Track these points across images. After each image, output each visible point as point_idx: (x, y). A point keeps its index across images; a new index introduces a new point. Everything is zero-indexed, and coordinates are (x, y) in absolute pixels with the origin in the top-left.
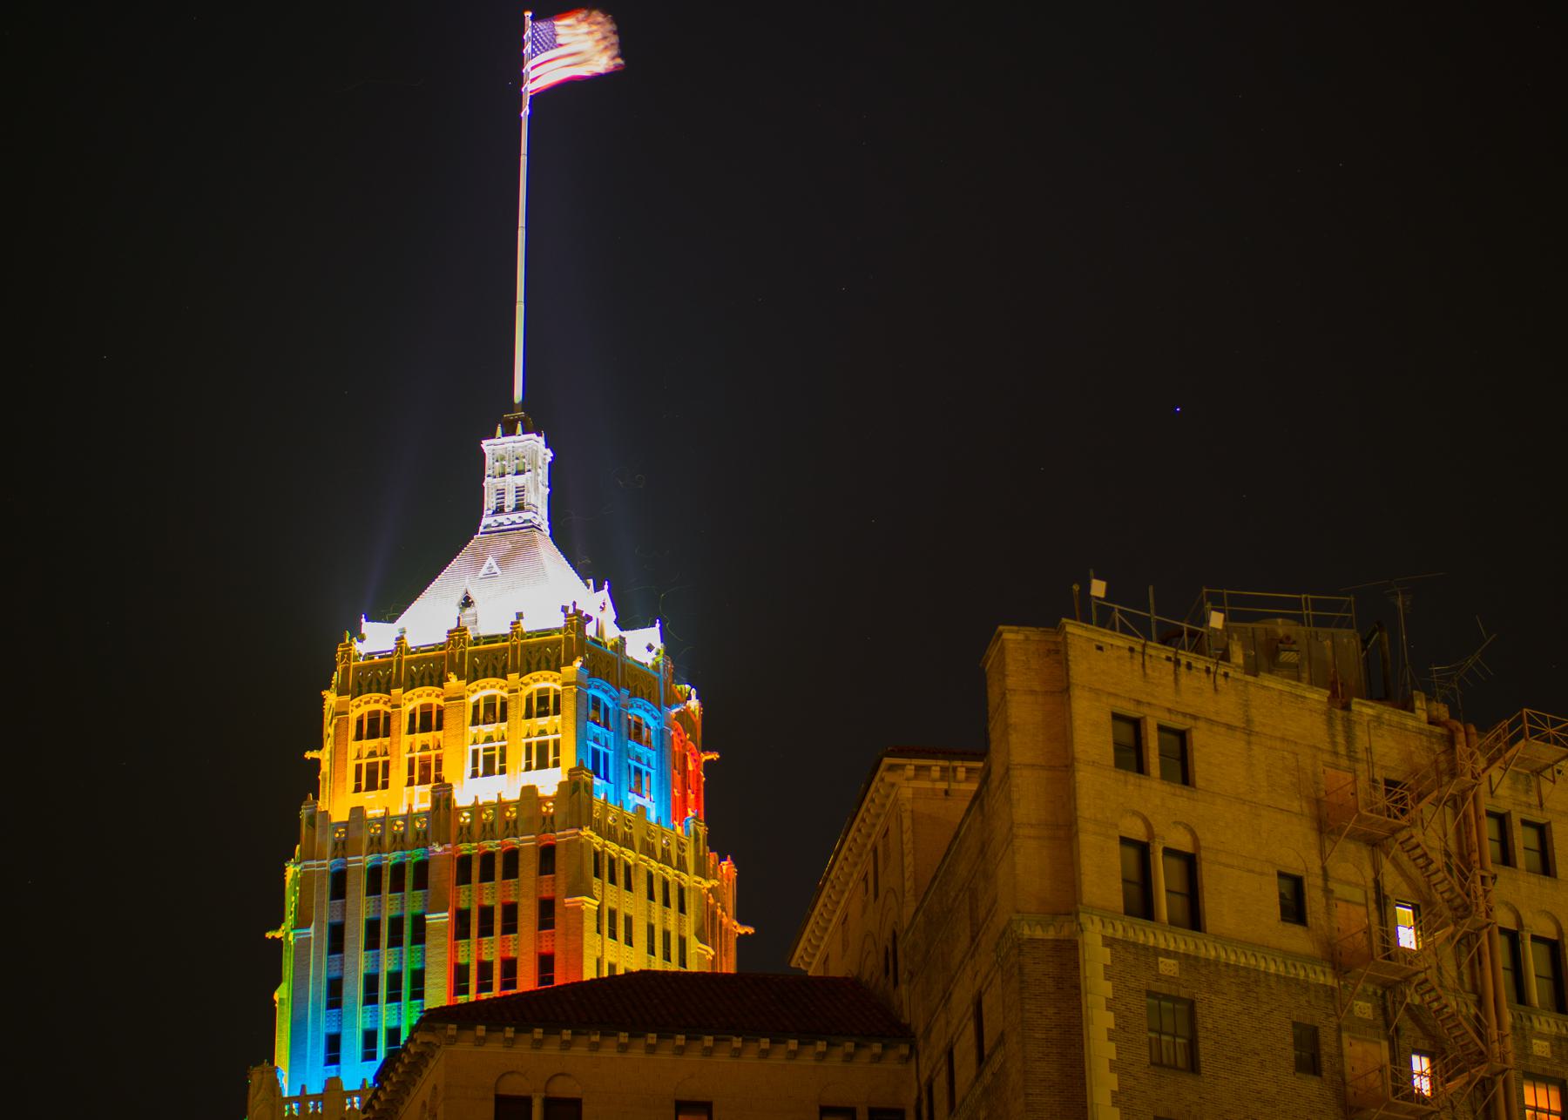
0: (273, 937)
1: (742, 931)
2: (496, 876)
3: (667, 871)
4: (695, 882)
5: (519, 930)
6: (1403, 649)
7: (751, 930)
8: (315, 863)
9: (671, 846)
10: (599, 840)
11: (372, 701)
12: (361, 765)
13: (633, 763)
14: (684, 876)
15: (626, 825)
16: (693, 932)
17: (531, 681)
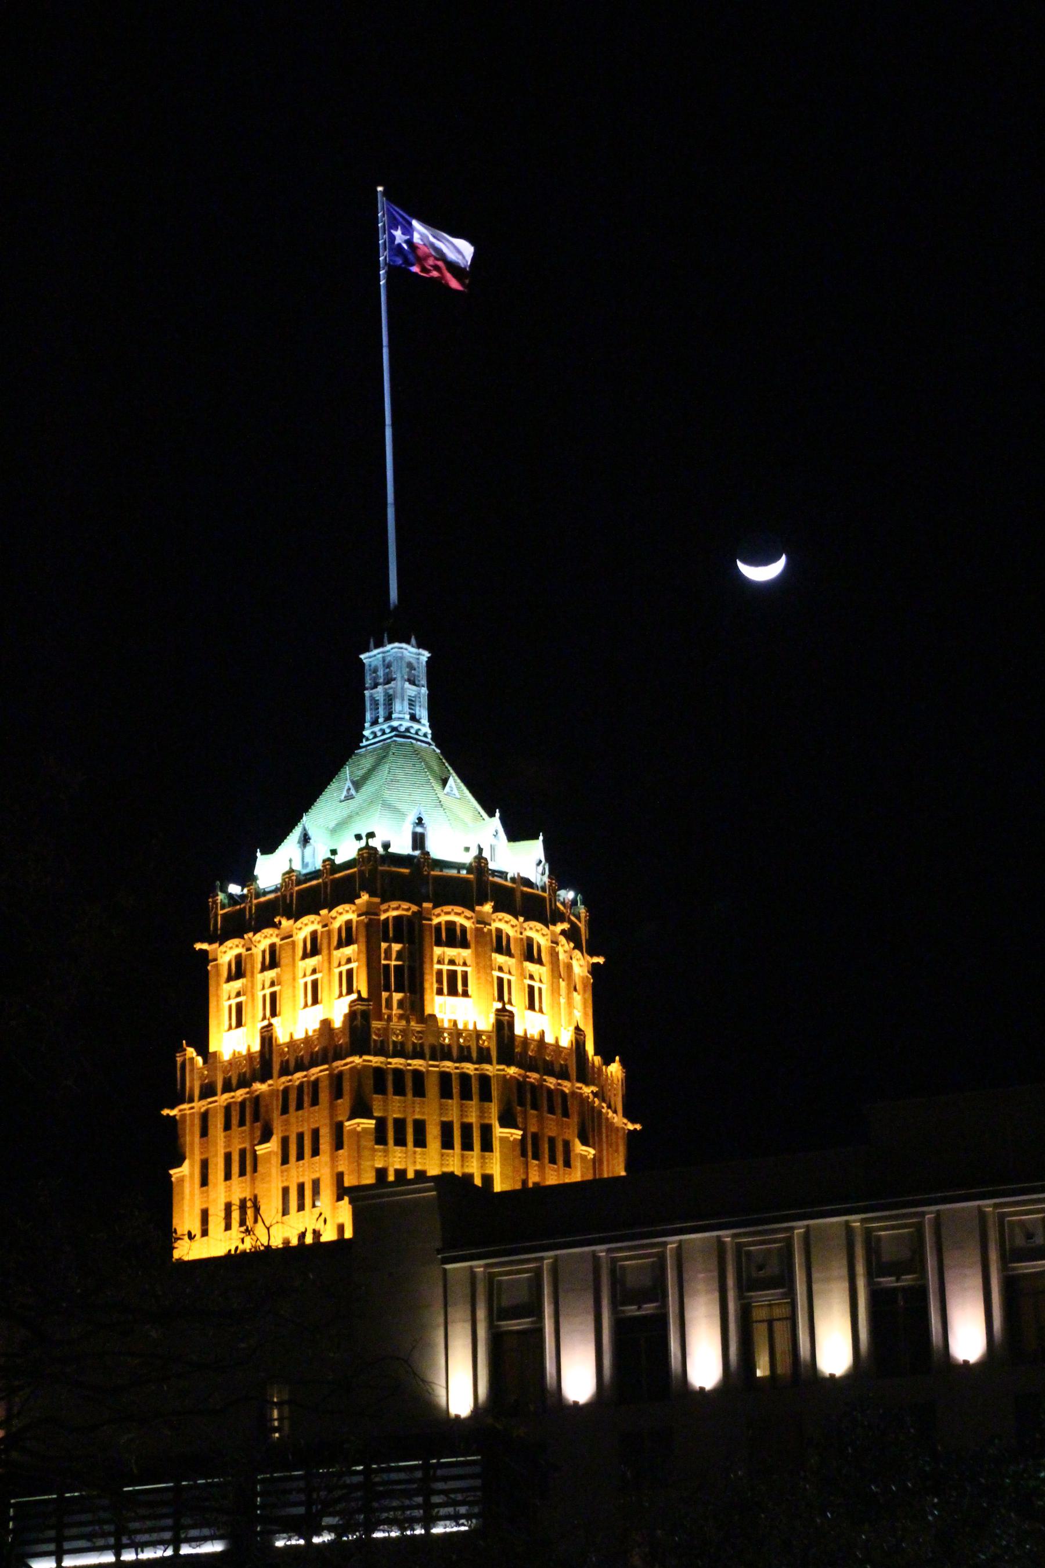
1: (631, 1127)
7: (638, 1127)
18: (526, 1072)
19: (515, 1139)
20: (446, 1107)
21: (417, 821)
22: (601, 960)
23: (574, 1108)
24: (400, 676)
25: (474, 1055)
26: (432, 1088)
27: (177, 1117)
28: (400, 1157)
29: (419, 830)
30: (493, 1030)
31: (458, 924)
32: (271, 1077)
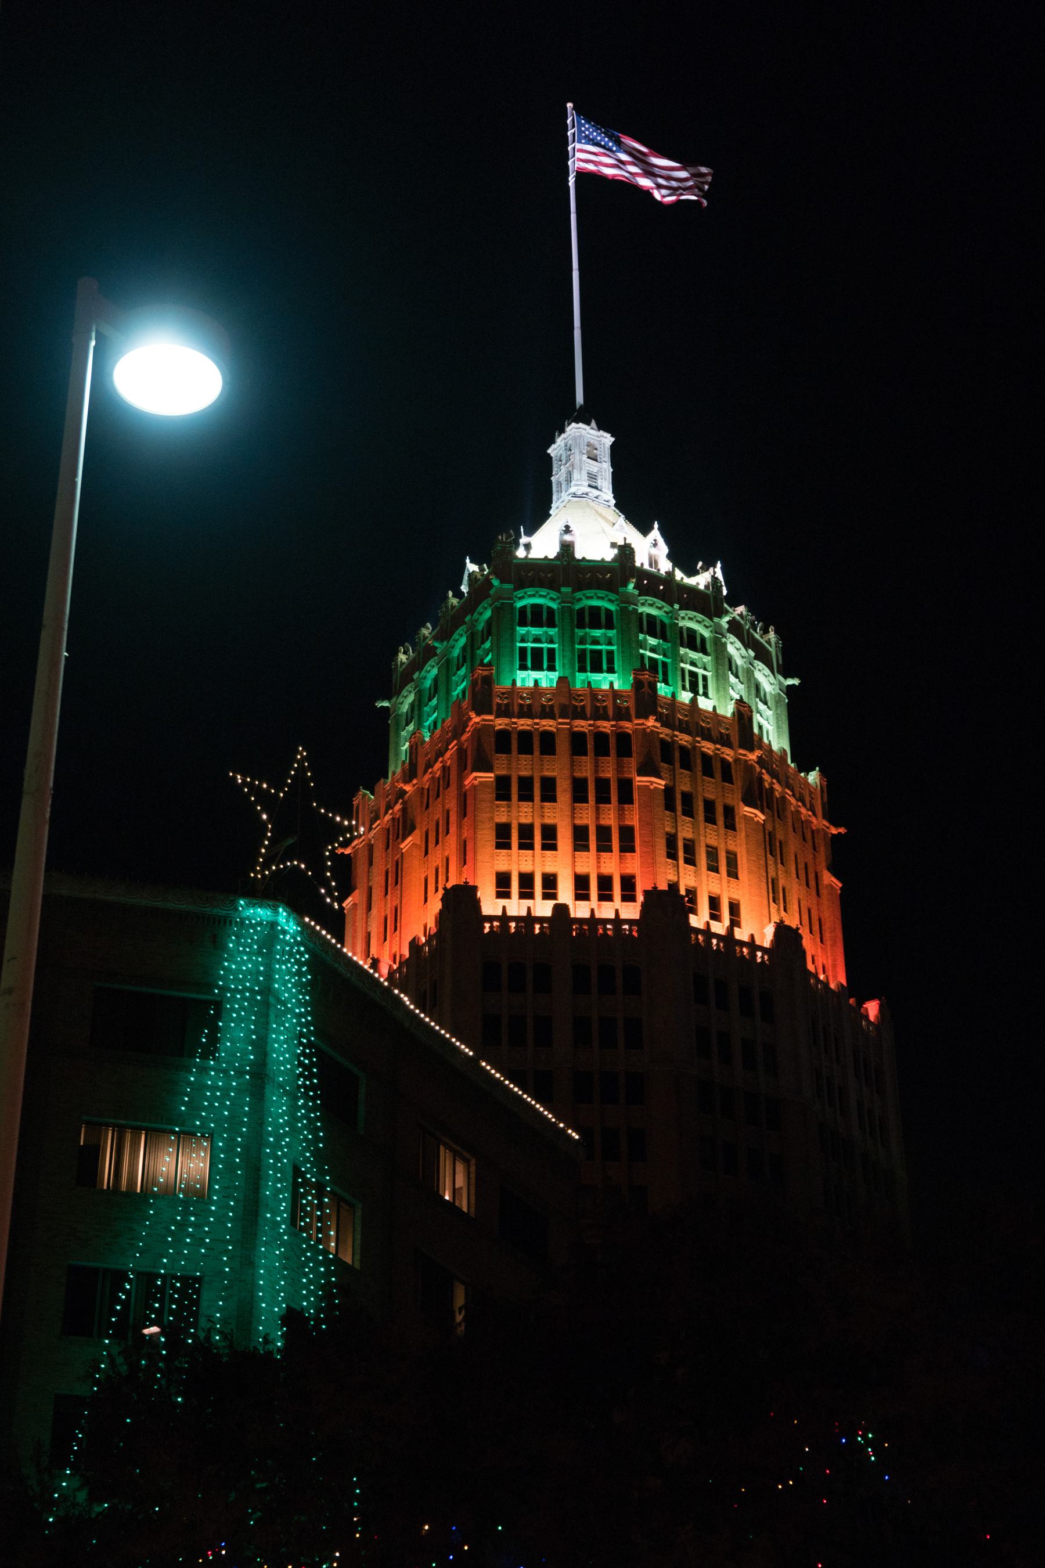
1: (834, 831)
6: (409, 843)
7: (842, 830)
10: (667, 731)
11: (549, 597)
13: (688, 667)
17: (583, 598)
18: (674, 731)
19: (656, 788)
20: (631, 817)
21: (564, 529)
22: (795, 682)
23: (737, 774)
24: (578, 451)
25: (611, 713)
26: (563, 745)
27: (352, 855)
28: (526, 812)
29: (567, 538)
30: (632, 690)
31: (603, 609)
32: (415, 777)
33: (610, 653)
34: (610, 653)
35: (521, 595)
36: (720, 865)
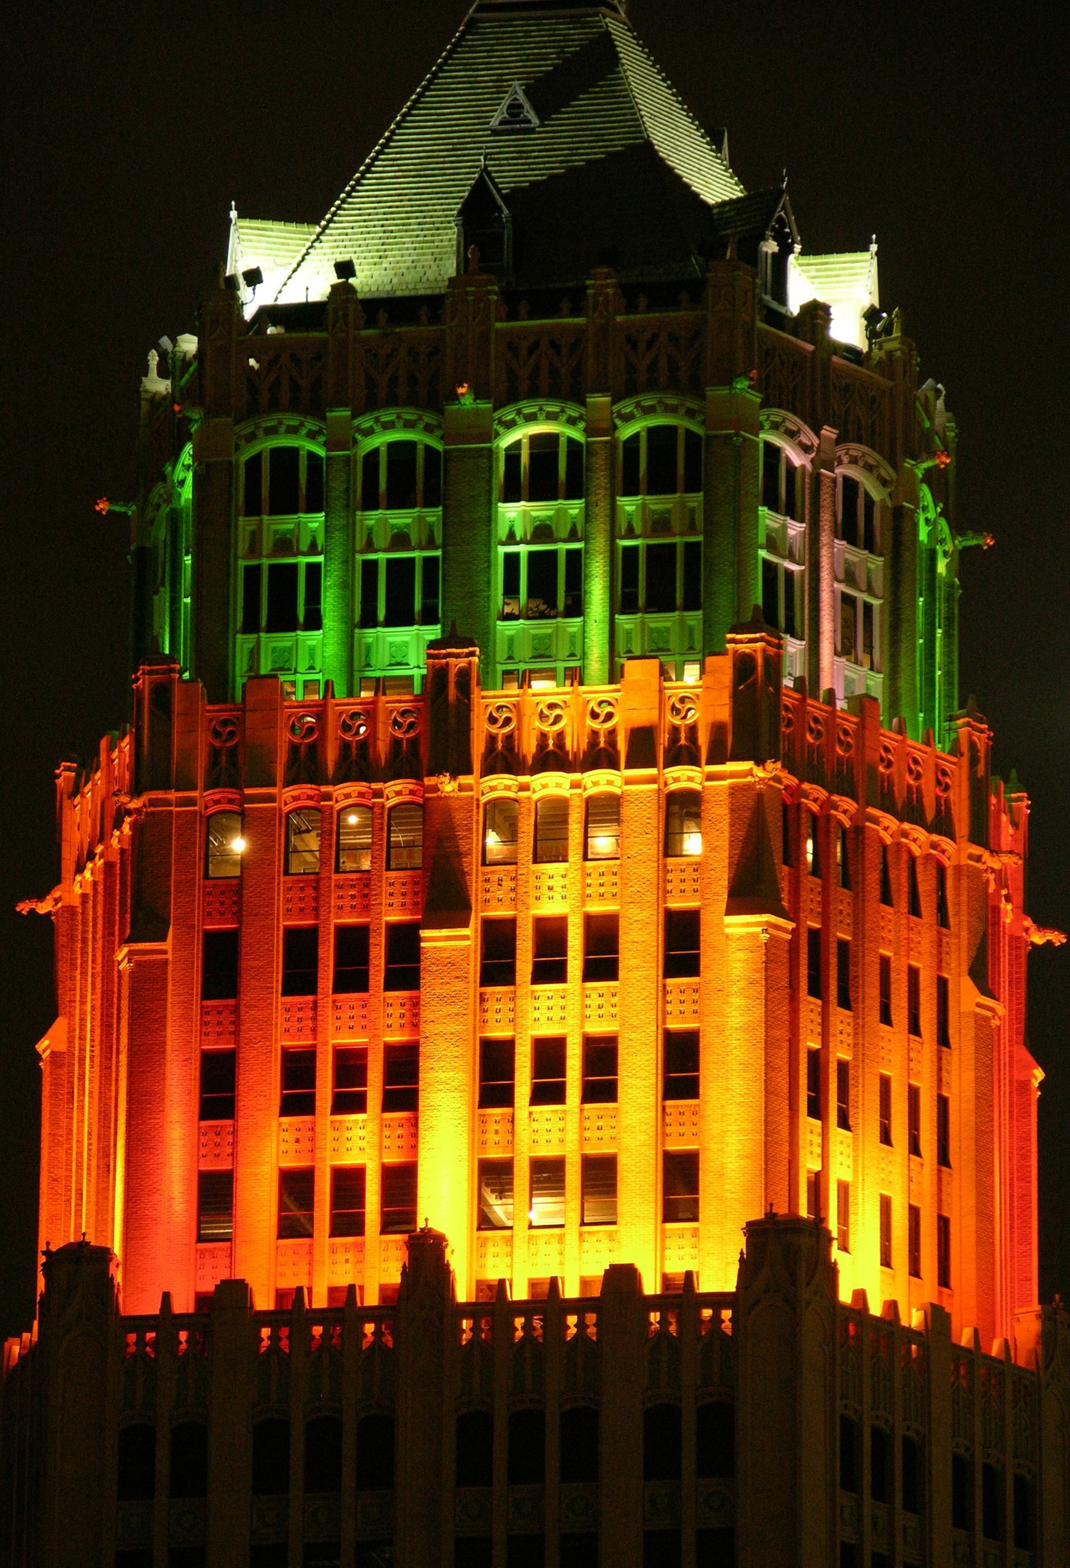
0: (32, 911)
1: (1038, 939)
2: (570, 853)
3: (944, 846)
4: (971, 857)
5: (621, 974)
7: (1057, 938)
8: (173, 795)
9: (923, 781)
11: (304, 432)
12: (258, 568)
14: (946, 843)
15: (911, 771)
16: (965, 967)
31: (420, 449)
32: (469, 772)
33: (314, 570)
34: (314, 570)
35: (368, 425)
36: (851, 1231)
